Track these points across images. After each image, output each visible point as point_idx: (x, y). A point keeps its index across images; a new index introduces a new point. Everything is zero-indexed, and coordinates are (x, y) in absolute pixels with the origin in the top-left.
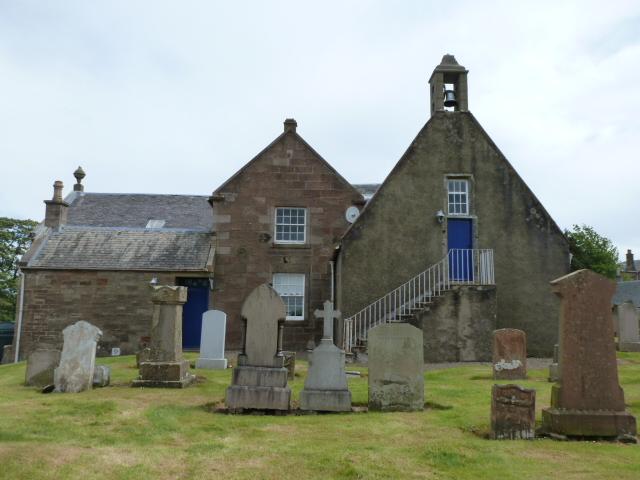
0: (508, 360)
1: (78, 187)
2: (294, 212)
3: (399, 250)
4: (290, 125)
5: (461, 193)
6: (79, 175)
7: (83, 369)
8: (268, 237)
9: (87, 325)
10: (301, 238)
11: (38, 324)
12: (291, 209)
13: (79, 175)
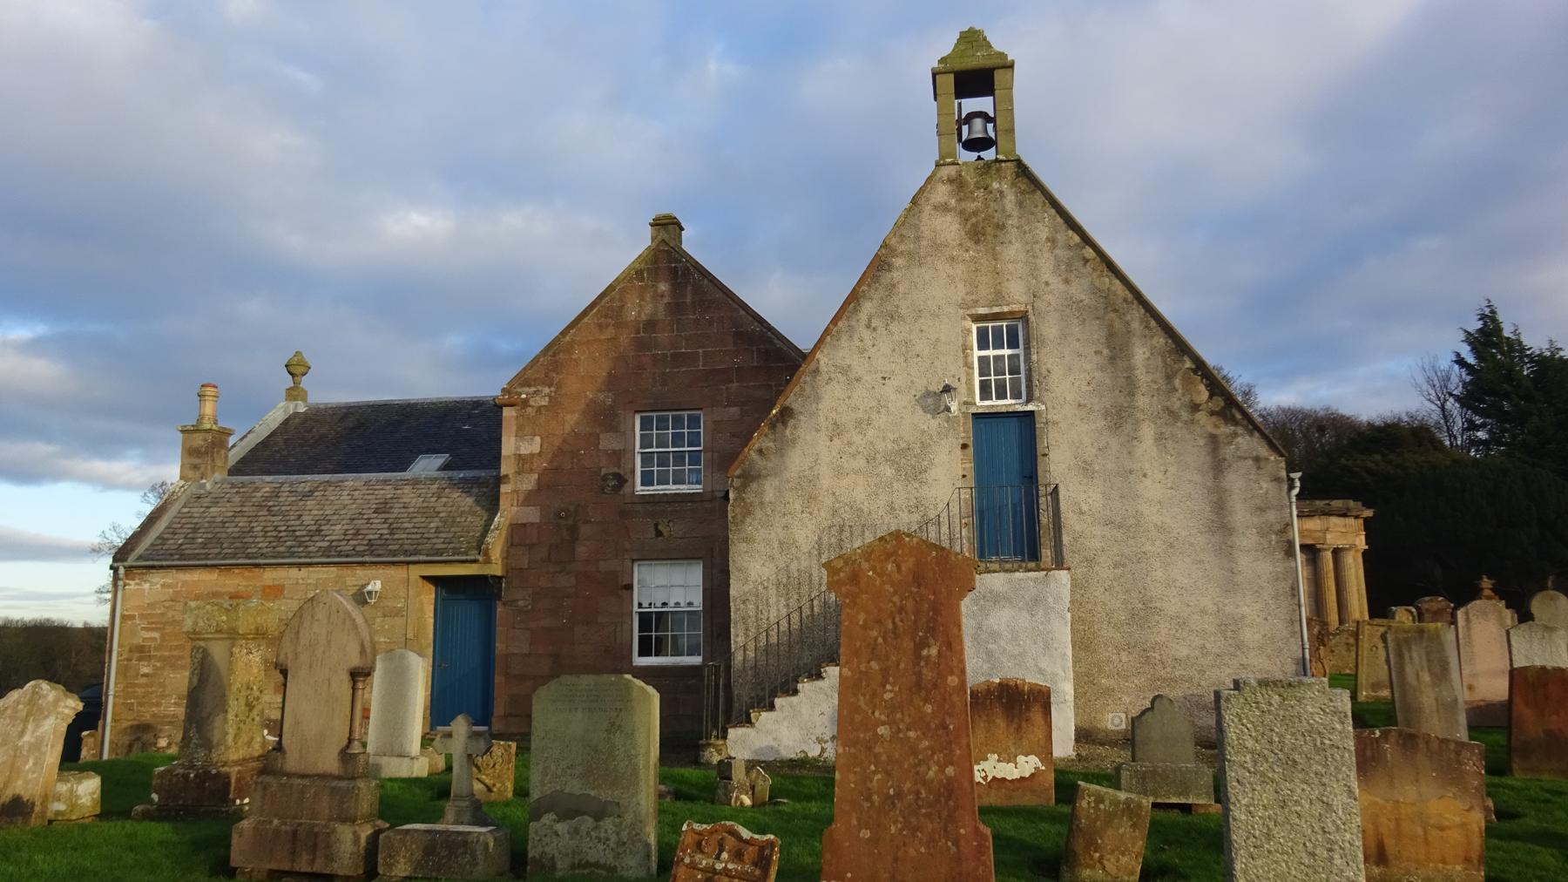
0: (1011, 759)
1: (294, 393)
2: (678, 422)
3: (860, 494)
4: (667, 226)
5: (991, 353)
6: (296, 368)
7: (26, 782)
8: (622, 480)
9: (45, 686)
10: (647, 480)
11: (147, 685)
12: (685, 414)
13: (296, 368)
